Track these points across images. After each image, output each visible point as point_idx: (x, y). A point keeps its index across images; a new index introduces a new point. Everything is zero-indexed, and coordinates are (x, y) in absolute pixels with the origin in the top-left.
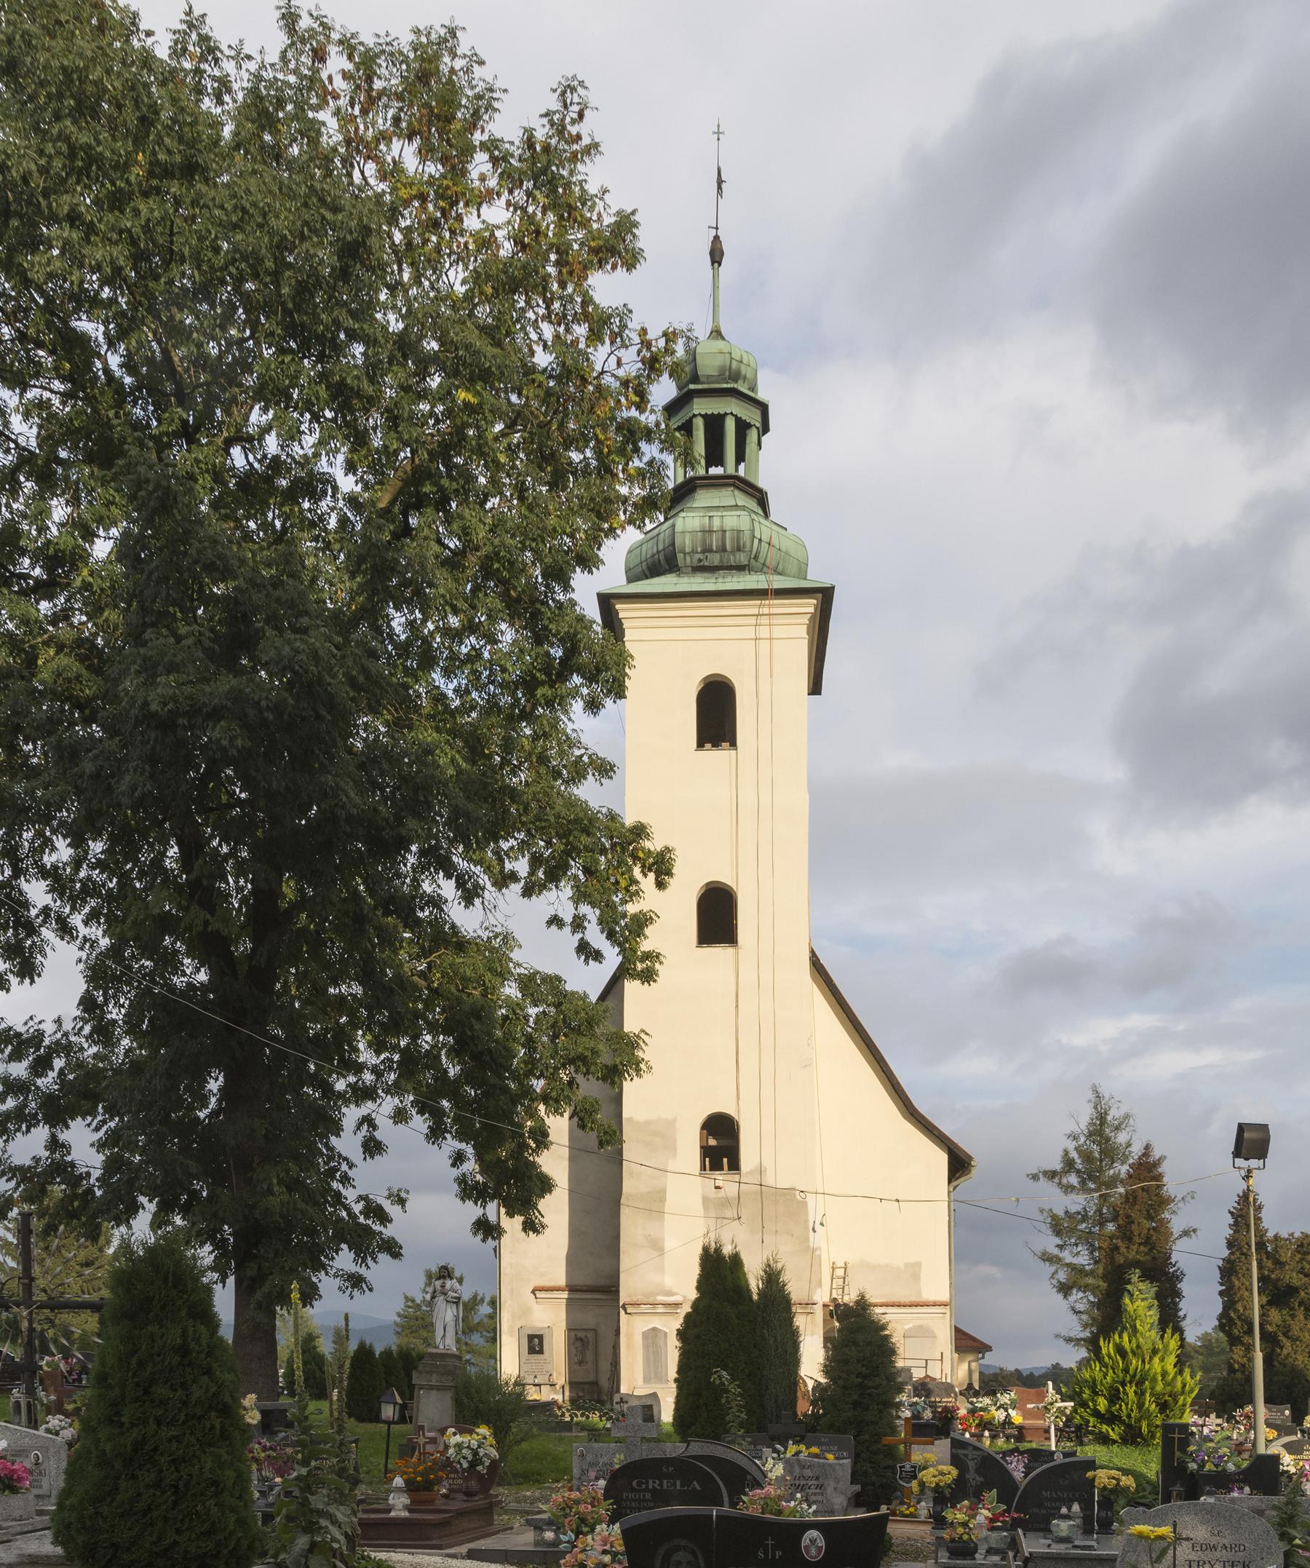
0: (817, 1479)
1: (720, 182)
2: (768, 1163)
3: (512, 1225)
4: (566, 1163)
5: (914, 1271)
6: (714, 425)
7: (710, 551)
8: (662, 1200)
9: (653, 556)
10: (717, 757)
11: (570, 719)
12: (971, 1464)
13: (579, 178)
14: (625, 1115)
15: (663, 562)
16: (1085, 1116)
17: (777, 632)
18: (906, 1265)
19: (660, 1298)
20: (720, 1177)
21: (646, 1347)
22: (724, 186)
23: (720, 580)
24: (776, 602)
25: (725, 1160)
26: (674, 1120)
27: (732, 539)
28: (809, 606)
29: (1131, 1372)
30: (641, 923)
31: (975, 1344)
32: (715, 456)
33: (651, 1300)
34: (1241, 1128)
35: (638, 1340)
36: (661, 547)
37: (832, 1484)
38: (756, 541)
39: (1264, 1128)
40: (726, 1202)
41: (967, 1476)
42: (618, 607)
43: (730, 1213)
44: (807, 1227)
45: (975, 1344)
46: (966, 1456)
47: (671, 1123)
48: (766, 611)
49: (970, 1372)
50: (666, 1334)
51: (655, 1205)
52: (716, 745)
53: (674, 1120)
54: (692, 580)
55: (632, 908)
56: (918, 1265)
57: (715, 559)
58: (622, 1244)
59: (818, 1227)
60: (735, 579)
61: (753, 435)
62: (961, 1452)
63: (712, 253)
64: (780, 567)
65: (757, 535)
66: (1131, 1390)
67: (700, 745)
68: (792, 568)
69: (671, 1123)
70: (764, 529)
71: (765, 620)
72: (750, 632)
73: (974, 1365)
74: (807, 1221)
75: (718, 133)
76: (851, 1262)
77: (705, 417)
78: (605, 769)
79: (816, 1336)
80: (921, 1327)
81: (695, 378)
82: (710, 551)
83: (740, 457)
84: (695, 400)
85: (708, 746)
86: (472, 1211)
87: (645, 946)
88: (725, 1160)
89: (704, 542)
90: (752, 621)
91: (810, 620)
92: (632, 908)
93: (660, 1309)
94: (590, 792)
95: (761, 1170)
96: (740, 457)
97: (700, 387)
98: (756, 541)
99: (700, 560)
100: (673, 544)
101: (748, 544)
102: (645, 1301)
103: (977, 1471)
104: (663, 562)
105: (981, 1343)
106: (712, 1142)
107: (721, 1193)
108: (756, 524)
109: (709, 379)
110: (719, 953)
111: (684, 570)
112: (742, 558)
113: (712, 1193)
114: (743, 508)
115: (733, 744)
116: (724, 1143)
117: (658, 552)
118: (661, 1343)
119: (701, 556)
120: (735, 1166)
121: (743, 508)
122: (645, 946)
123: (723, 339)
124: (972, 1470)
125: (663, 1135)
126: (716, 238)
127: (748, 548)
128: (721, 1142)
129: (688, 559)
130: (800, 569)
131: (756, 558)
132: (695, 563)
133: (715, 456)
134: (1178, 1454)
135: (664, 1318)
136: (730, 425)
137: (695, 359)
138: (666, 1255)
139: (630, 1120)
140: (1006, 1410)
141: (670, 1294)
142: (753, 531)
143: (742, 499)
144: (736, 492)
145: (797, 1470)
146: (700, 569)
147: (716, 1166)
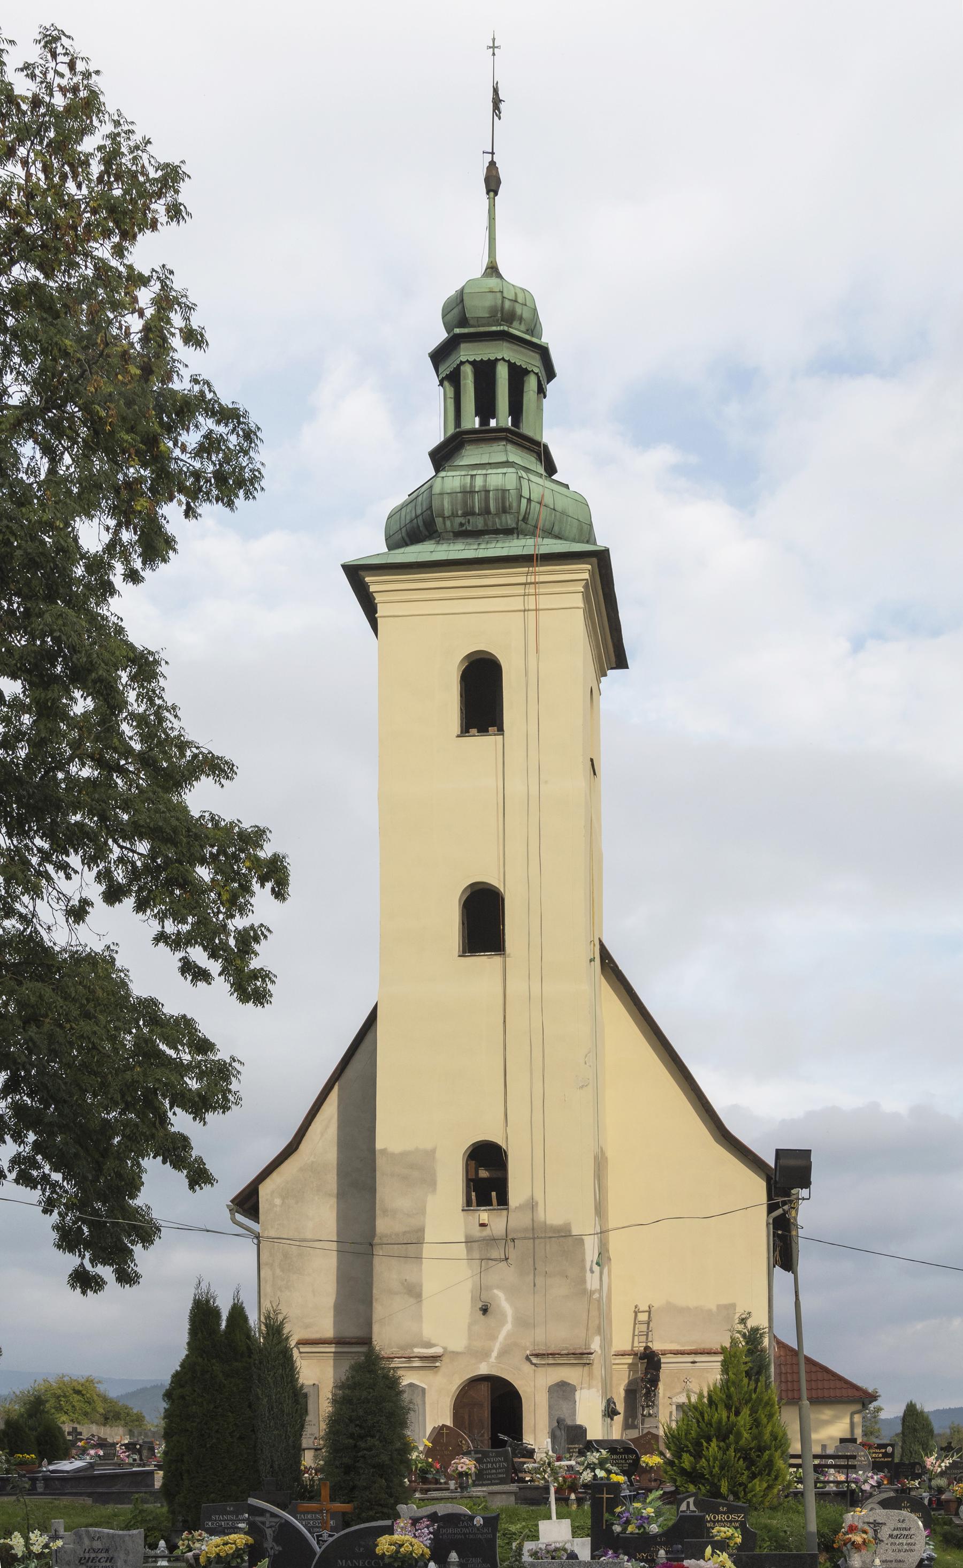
0: (107, 1551)
1: (497, 102)
2: (539, 1197)
3: (106, 1272)
6: (485, 372)
7: (472, 513)
8: (420, 1242)
9: (412, 521)
10: (483, 745)
11: (176, 716)
12: (269, 1532)
13: (126, 128)
14: (379, 1145)
16: (429, 1146)
17: (544, 602)
18: (719, 1307)
19: (419, 1351)
20: (484, 1216)
23: (483, 546)
24: (542, 569)
25: (494, 1194)
26: (434, 1151)
27: (496, 499)
28: (583, 572)
32: (486, 408)
34: (777, 1151)
36: (419, 512)
37: (122, 1556)
38: (524, 502)
39: (806, 1154)
41: (265, 1545)
42: (367, 579)
45: (857, 1394)
46: (263, 1523)
47: (430, 1154)
48: (531, 579)
50: (423, 1390)
51: (412, 1244)
52: (483, 730)
53: (434, 1151)
54: (452, 547)
55: (238, 923)
57: (478, 523)
60: (499, 545)
61: (531, 384)
63: (487, 180)
64: (556, 529)
65: (525, 493)
67: (465, 730)
69: (430, 1154)
72: (517, 603)
74: (583, 1260)
75: (494, 47)
76: (656, 1305)
77: (473, 363)
78: (218, 768)
79: (594, 1390)
82: (472, 513)
83: (516, 409)
86: (71, 1261)
87: (255, 964)
88: (494, 1194)
89: (465, 503)
90: (520, 590)
92: (238, 923)
95: (532, 1205)
96: (516, 409)
97: (465, 330)
98: (524, 502)
99: (461, 525)
100: (430, 508)
101: (515, 505)
103: (275, 1540)
105: (865, 1392)
108: (525, 483)
109: (479, 321)
110: (486, 963)
112: (509, 521)
115: (501, 730)
117: (417, 517)
119: (462, 520)
120: (503, 1201)
121: (507, 464)
124: (270, 1538)
125: (420, 1170)
126: (492, 164)
127: (514, 510)
128: (487, 1173)
129: (448, 523)
130: (581, 530)
131: (525, 519)
133: (486, 408)
136: (502, 373)
137: (462, 301)
139: (384, 1151)
140: (593, 1470)
141: (429, 1345)
143: (515, 455)
144: (509, 447)
145: (87, 1542)
146: (463, 534)
147: (484, 1201)
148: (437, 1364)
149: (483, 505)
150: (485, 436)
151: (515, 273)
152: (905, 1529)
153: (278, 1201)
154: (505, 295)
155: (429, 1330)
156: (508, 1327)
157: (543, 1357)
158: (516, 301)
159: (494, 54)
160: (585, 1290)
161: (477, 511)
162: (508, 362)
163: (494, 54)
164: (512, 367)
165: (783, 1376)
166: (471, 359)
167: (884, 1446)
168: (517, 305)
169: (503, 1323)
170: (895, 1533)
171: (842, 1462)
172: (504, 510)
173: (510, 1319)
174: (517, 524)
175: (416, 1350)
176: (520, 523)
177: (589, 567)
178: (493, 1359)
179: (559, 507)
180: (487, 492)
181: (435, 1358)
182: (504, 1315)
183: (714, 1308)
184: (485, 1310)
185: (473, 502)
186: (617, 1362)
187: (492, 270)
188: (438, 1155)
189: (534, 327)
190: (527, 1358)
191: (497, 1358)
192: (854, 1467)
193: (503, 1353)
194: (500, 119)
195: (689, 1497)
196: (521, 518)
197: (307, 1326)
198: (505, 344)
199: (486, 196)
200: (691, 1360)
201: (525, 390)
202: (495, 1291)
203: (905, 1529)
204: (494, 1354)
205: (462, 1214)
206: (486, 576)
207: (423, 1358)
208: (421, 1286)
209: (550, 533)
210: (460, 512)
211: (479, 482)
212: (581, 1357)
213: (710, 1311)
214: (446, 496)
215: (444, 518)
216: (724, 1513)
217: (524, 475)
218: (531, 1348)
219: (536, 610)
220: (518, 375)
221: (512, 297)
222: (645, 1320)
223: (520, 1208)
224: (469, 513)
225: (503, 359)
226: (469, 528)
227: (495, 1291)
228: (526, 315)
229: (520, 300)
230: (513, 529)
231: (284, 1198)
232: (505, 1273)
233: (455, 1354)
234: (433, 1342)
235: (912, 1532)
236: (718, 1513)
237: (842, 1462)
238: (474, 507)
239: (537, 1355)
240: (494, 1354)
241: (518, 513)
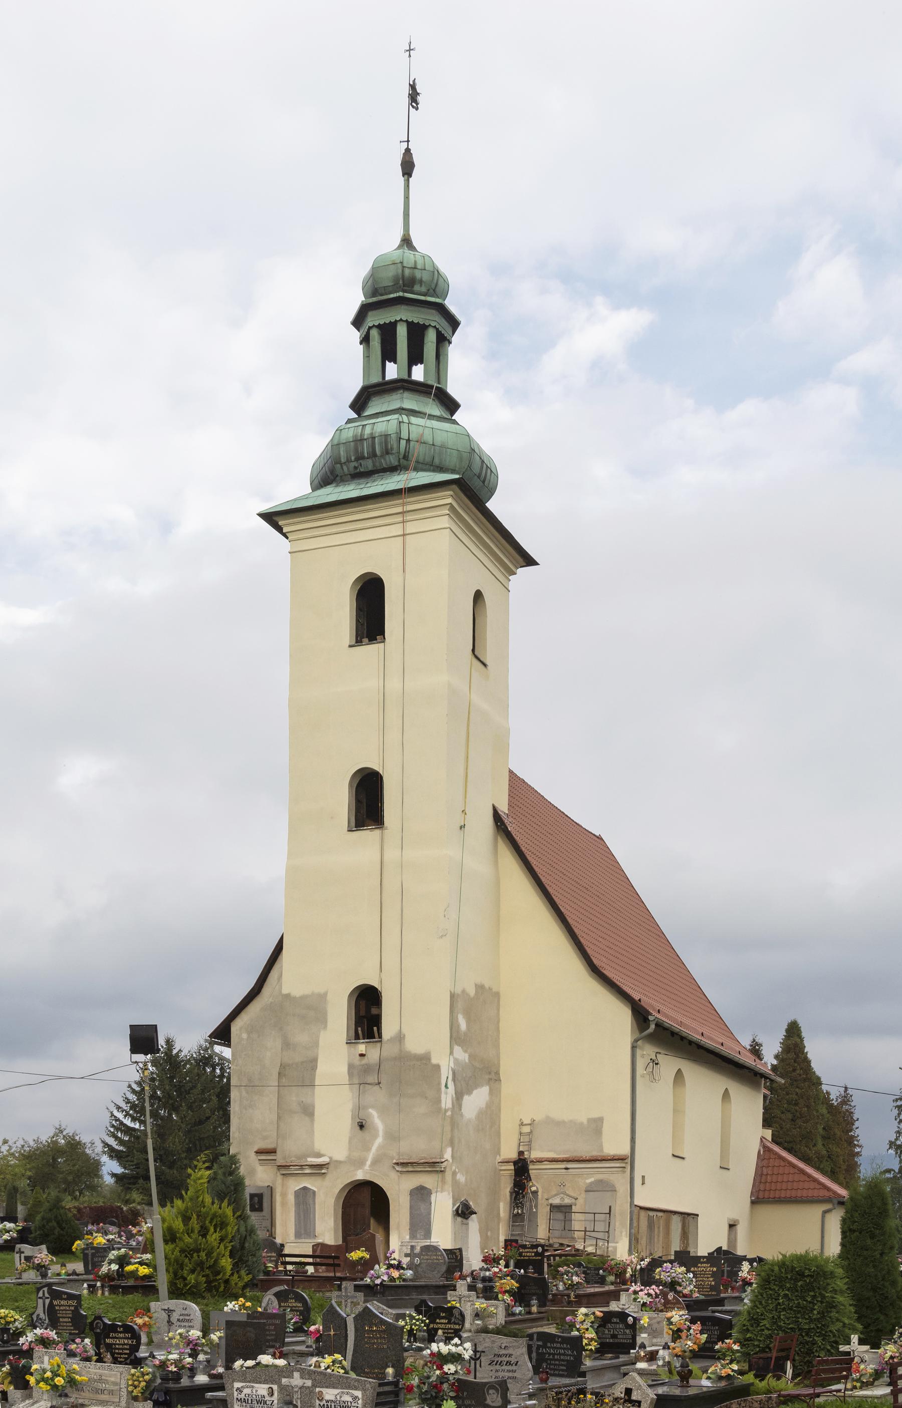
5: (596, 1126)
6: (388, 332)
7: (363, 458)
16: (322, 991)
17: (410, 528)
18: (589, 1120)
20: (362, 1048)
21: (297, 1204)
22: (419, 98)
24: (408, 500)
27: (381, 443)
31: (827, 1194)
35: (291, 1198)
38: (403, 443)
43: (372, 1079)
45: (827, 1194)
47: (323, 997)
50: (314, 1192)
53: (326, 994)
56: (601, 1120)
57: (368, 465)
61: (431, 337)
65: (405, 435)
69: (323, 997)
72: (397, 530)
77: (379, 327)
79: (445, 1193)
80: (601, 1181)
82: (363, 458)
90: (399, 518)
95: (400, 1038)
98: (403, 443)
99: (355, 468)
101: (395, 446)
107: (365, 1061)
108: (404, 427)
110: (369, 835)
112: (392, 460)
113: (357, 1060)
118: (311, 1202)
119: (355, 464)
125: (313, 1010)
126: (408, 151)
128: (367, 1008)
129: (345, 468)
131: (406, 457)
132: (352, 471)
136: (402, 332)
141: (319, 1155)
143: (409, 401)
148: (323, 1171)
149: (371, 450)
152: (187, 1315)
153: (245, 1036)
154: (405, 265)
155: (319, 1144)
156: (379, 1140)
157: (406, 1166)
158: (415, 268)
159: (410, 56)
160: (440, 1108)
162: (407, 321)
163: (410, 56)
164: (411, 326)
165: (764, 1177)
166: (376, 324)
167: (536, 1246)
168: (416, 271)
169: (376, 1136)
170: (181, 1318)
171: (331, 1261)
172: (387, 452)
173: (381, 1133)
174: (399, 461)
175: (309, 1159)
176: (402, 461)
177: (451, 493)
178: (367, 1167)
179: (438, 442)
180: (374, 438)
181: (320, 1166)
182: (377, 1130)
183: (585, 1122)
185: (363, 448)
186: (503, 1168)
187: (407, 242)
188: (329, 997)
191: (370, 1166)
192: (339, 1265)
193: (375, 1162)
194: (417, 109)
195: (44, 1286)
196: (401, 456)
197: (265, 1138)
198: (403, 307)
199: (403, 179)
200: (563, 1166)
202: (370, 1110)
203: (187, 1315)
204: (368, 1163)
205: (346, 1046)
206: (371, 510)
207: (312, 1166)
208: (314, 1107)
209: (421, 466)
210: (353, 458)
211: (368, 430)
212: (433, 1166)
213: (582, 1123)
214: (341, 446)
216: (65, 1299)
217: (405, 418)
218: (397, 1157)
219: (404, 535)
220: (417, 332)
221: (411, 265)
222: (528, 1133)
223: (391, 1040)
224: (360, 458)
225: (401, 320)
227: (370, 1110)
228: (426, 277)
229: (419, 267)
231: (249, 1033)
232: (377, 1095)
233: (339, 1162)
234: (322, 1152)
235: (191, 1317)
236: (62, 1299)
237: (331, 1261)
238: (363, 453)
239: (402, 1164)
240: (368, 1163)
241: (399, 453)
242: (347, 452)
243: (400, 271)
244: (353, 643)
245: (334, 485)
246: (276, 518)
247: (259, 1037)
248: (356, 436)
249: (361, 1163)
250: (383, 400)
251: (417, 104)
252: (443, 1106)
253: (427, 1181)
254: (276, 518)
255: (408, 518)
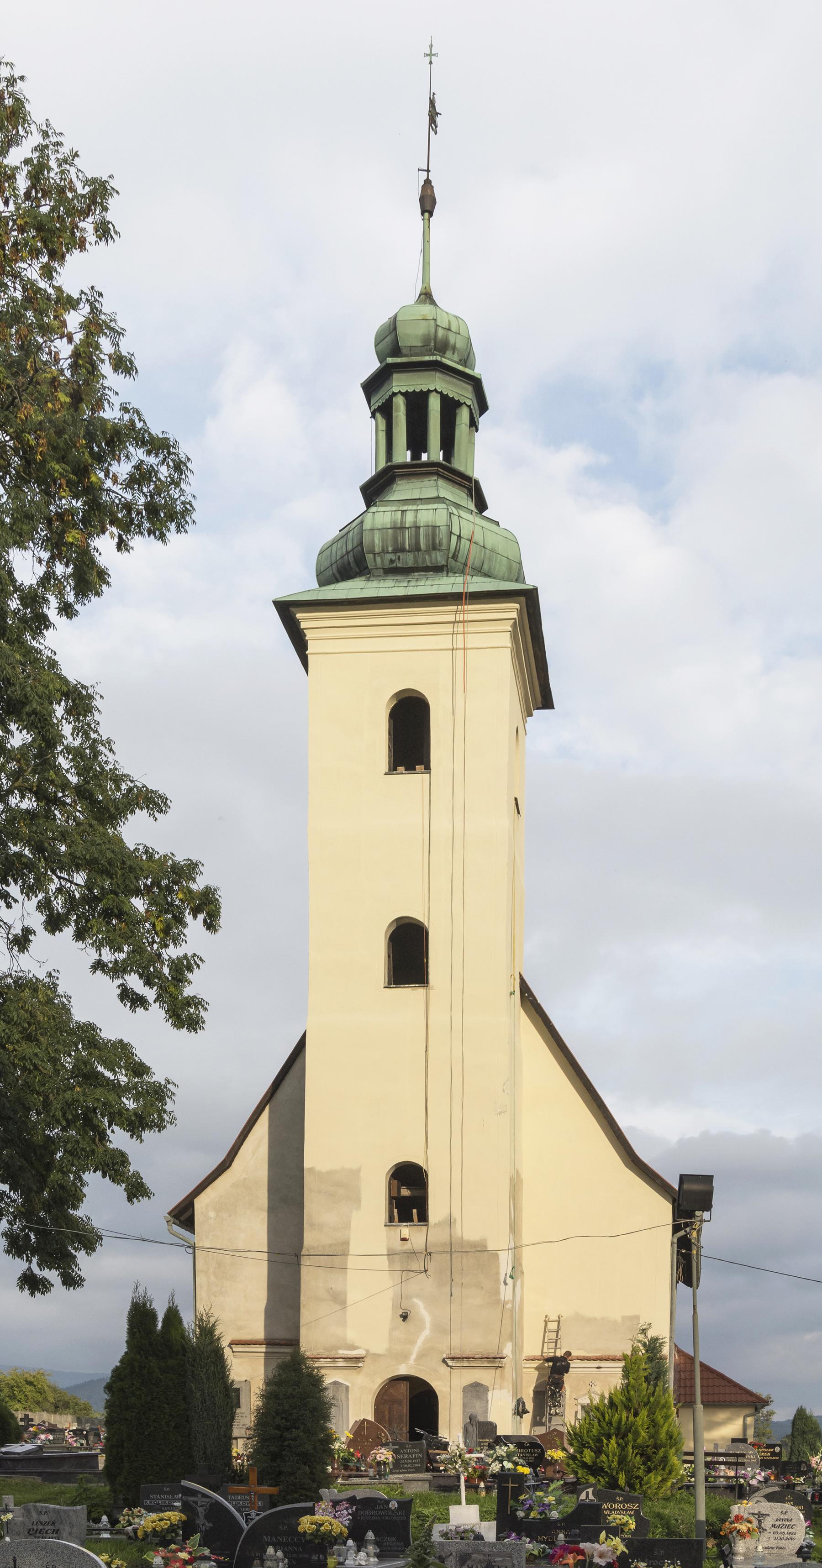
0: (53, 1523)
1: (433, 115)
2: (456, 1214)
4: (265, 1215)
6: (417, 403)
7: (403, 550)
9: (342, 557)
11: (111, 750)
14: (307, 1165)
15: (353, 565)
17: (473, 641)
18: (624, 1318)
20: (405, 1230)
22: (439, 119)
25: (415, 1211)
27: (427, 536)
28: (511, 610)
29: (615, 1424)
30: (182, 968)
31: (750, 1399)
32: (417, 443)
33: (332, 1354)
36: (350, 548)
37: (67, 1529)
38: (454, 539)
39: (709, 1179)
40: (412, 1254)
42: (298, 616)
43: (417, 1265)
44: (498, 1280)
45: (750, 1399)
46: (196, 1503)
47: (355, 1173)
48: (460, 617)
49: (745, 1427)
50: (347, 1388)
51: (337, 1255)
53: (359, 1171)
55: (172, 952)
57: (408, 560)
58: (302, 1298)
59: (509, 1281)
60: (429, 582)
61: (463, 416)
62: (191, 1499)
63: (422, 200)
65: (456, 530)
66: (613, 1444)
67: (393, 768)
68: (501, 568)
69: (355, 1173)
70: (467, 523)
71: (460, 628)
72: (445, 642)
73: (750, 1420)
74: (498, 1274)
75: (430, 55)
77: (406, 394)
78: (152, 801)
79: (505, 1391)
81: (396, 350)
82: (403, 550)
83: (448, 443)
84: (395, 376)
85: (401, 769)
86: (20, 1266)
88: (415, 1211)
89: (395, 539)
90: (449, 628)
91: (514, 626)
92: (172, 952)
93: (341, 1363)
94: (136, 831)
95: (450, 1222)
98: (454, 539)
99: (392, 561)
101: (445, 541)
102: (326, 1354)
104: (353, 565)
106: (405, 1192)
108: (455, 519)
110: (410, 994)
111: (376, 572)
112: (439, 558)
114: (438, 499)
115: (428, 768)
116: (417, 1193)
117: (347, 553)
118: (343, 1397)
120: (423, 1218)
121: (438, 499)
122: (188, 991)
123: (433, 302)
124: (201, 1516)
125: (346, 1188)
126: (428, 182)
127: (444, 547)
128: (409, 1192)
129: (378, 559)
131: (455, 557)
132: (387, 565)
133: (417, 443)
134: (511, 1503)
135: (345, 1372)
137: (395, 329)
138: (349, 1310)
139: (311, 1170)
140: (501, 1462)
142: (450, 526)
143: (446, 490)
144: (441, 482)
145: (34, 1515)
146: (393, 571)
147: (405, 1218)
148: (360, 1365)
149: (414, 541)
150: (416, 470)
151: (452, 303)
153: (212, 1214)
154: (438, 323)
156: (426, 1333)
158: (449, 329)
159: (431, 63)
160: (498, 1301)
161: (407, 548)
162: (441, 393)
163: (431, 63)
166: (403, 391)
170: (778, 1523)
171: (733, 1459)
172: (434, 547)
173: (428, 1325)
174: (447, 561)
178: (412, 1361)
181: (358, 1359)
183: (619, 1319)
184: (405, 1317)
186: (528, 1366)
187: (426, 296)
189: (467, 359)
190: (444, 1361)
193: (421, 1356)
194: (436, 133)
196: (450, 555)
198: (438, 374)
201: (457, 423)
202: (415, 1300)
204: (413, 1357)
205: (385, 1229)
208: (345, 1294)
210: (390, 549)
211: (409, 518)
212: (494, 1360)
214: (377, 532)
215: (375, 554)
216: (621, 1502)
217: (455, 511)
220: (450, 407)
221: (445, 325)
222: (554, 1329)
223: (438, 1225)
224: (399, 549)
225: (435, 390)
226: (399, 565)
230: (443, 566)
233: (376, 1357)
234: (357, 1344)
236: (615, 1502)
237: (733, 1459)
240: (413, 1357)
242: (383, 540)
243: (433, 330)
244: (390, 770)
245: (363, 578)
246: (293, 609)
247: (230, 1216)
248: (395, 522)
249: (404, 1357)
250: (411, 485)
251: (436, 127)
252: (502, 1297)
253: (483, 1376)
254: (293, 609)
255: (470, 629)
